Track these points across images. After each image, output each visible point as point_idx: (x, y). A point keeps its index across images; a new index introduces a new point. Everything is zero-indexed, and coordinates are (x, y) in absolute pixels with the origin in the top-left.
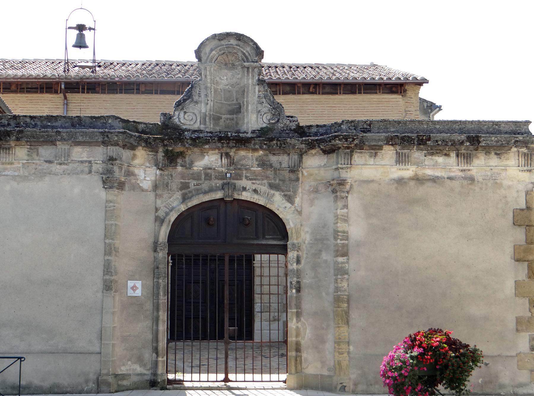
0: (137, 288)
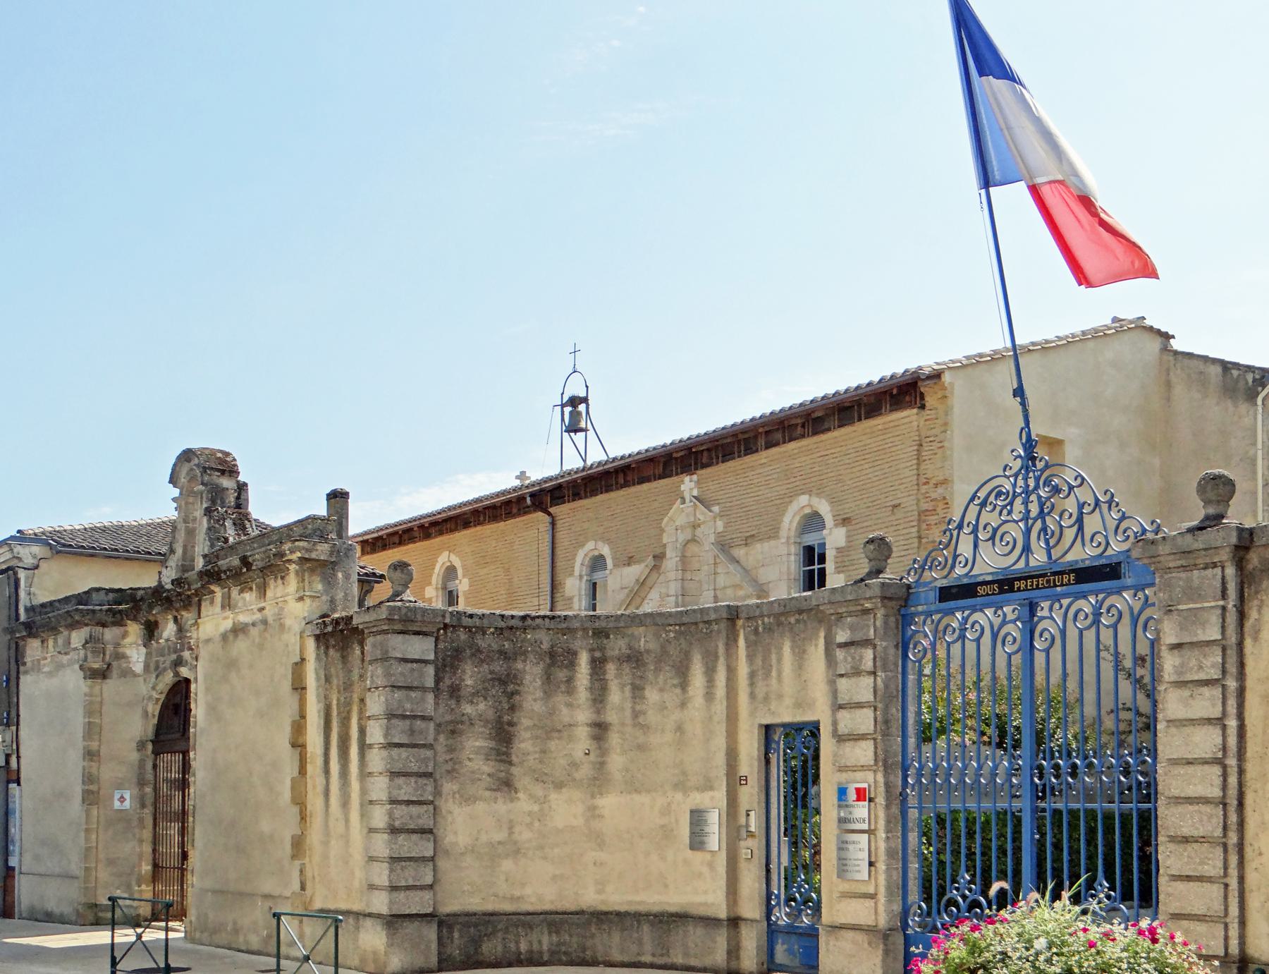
0: (118, 800)
